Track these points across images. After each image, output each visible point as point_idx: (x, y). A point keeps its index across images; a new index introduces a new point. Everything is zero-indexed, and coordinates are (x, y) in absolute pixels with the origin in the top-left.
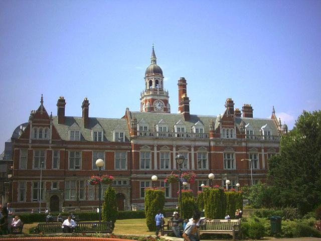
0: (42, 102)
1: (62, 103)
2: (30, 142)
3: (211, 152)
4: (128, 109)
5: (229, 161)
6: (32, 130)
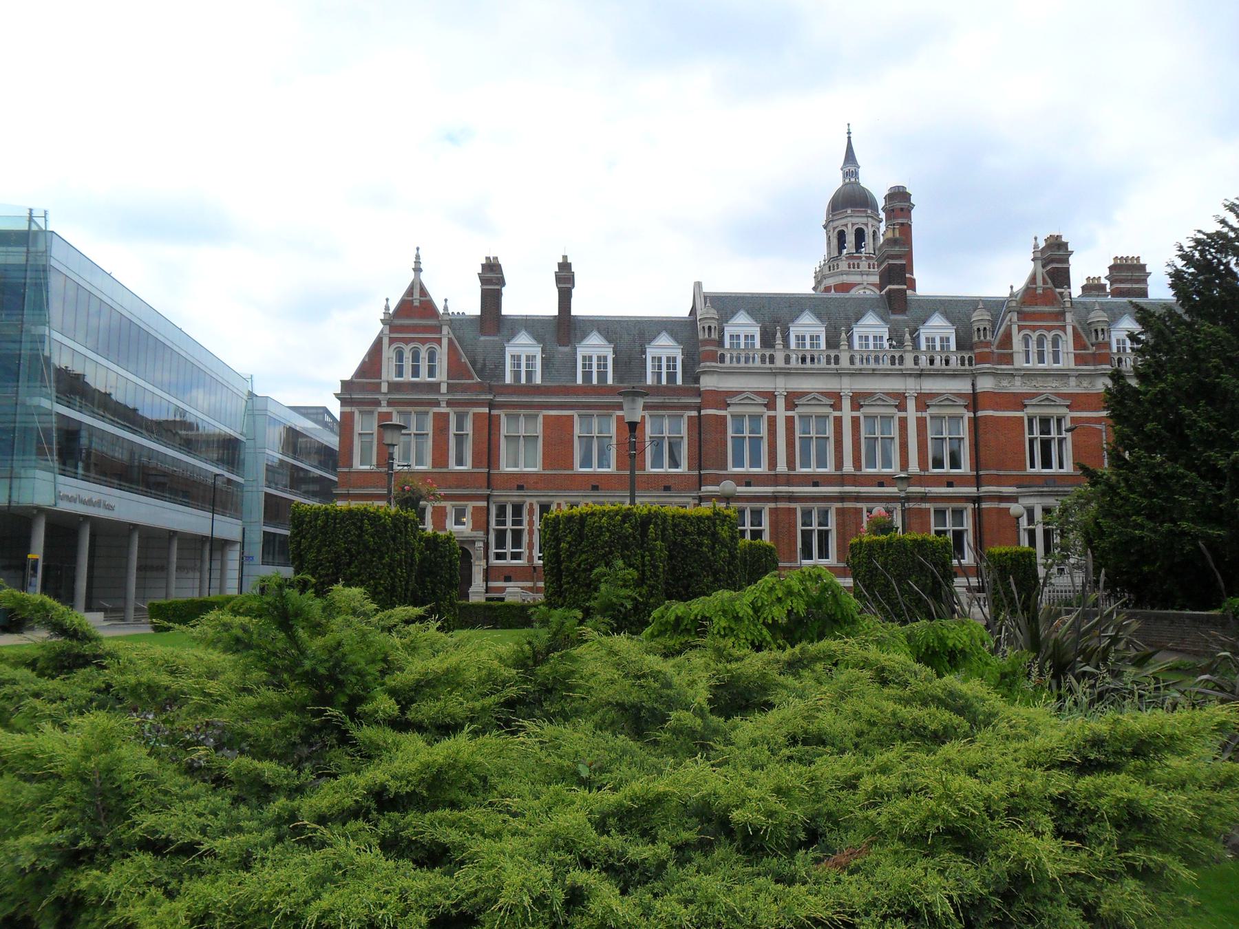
0: (418, 270)
1: (492, 276)
2: (384, 388)
5: (1046, 445)
6: (388, 353)
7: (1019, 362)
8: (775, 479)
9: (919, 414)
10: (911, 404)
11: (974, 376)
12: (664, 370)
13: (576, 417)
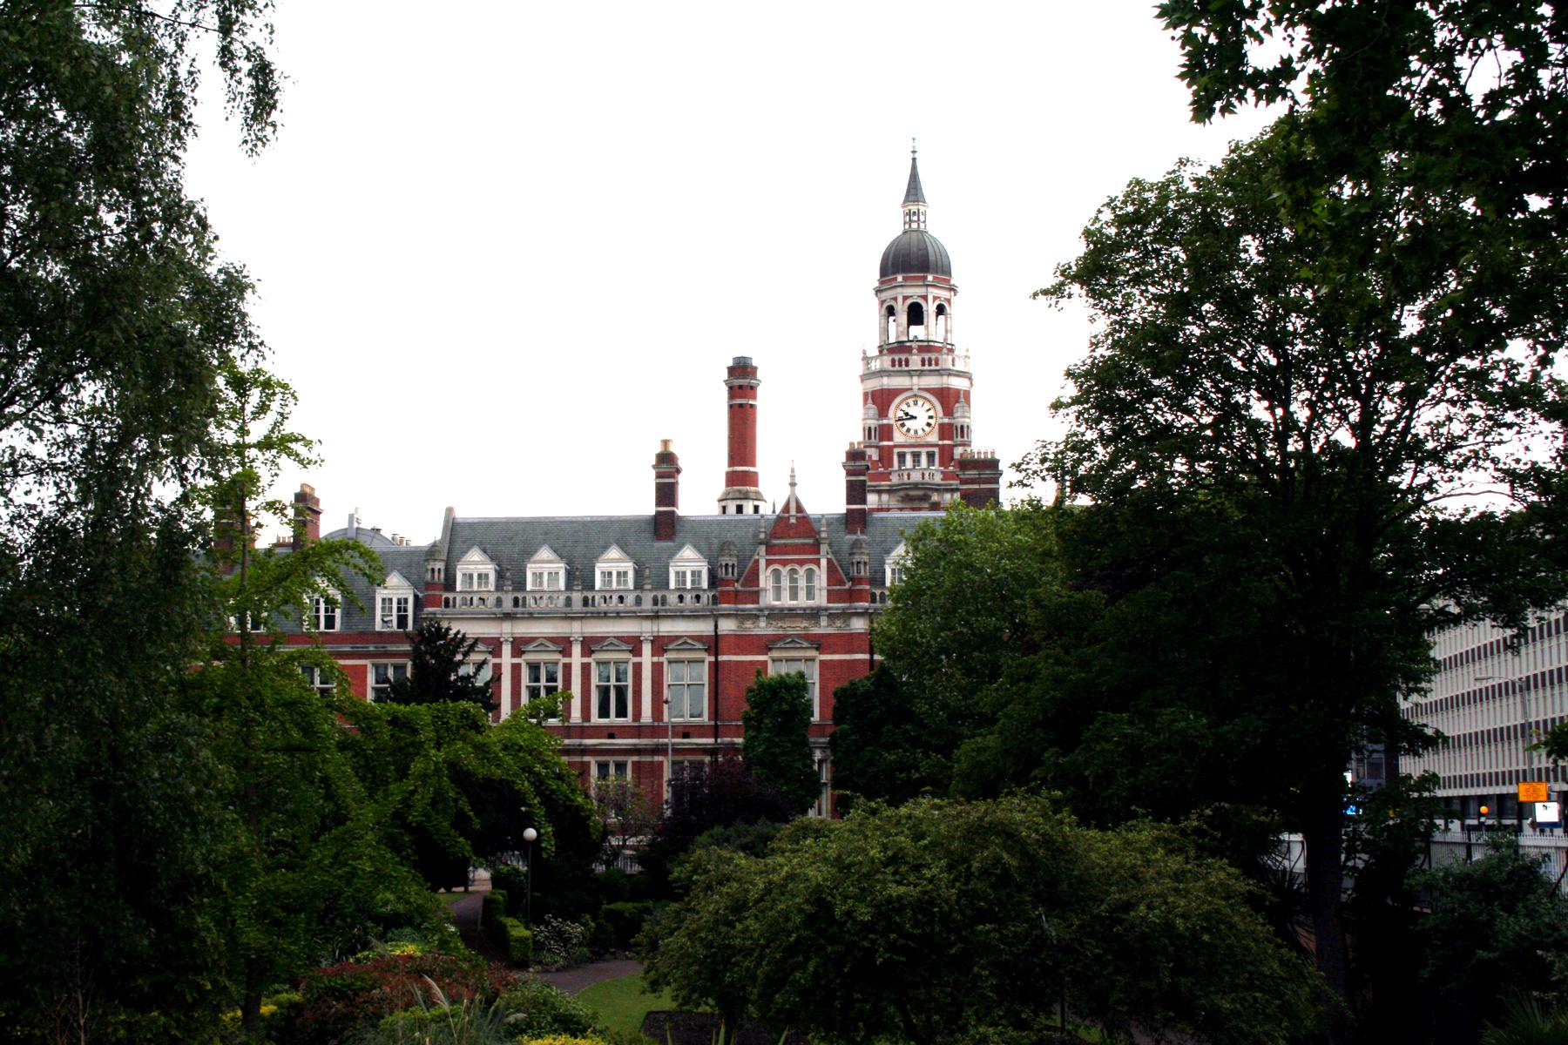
3: (722, 658)
4: (450, 511)
7: (768, 599)
8: (638, 731)
9: (656, 659)
10: (647, 649)
11: (716, 618)
12: (322, 613)
13: (593, 665)
